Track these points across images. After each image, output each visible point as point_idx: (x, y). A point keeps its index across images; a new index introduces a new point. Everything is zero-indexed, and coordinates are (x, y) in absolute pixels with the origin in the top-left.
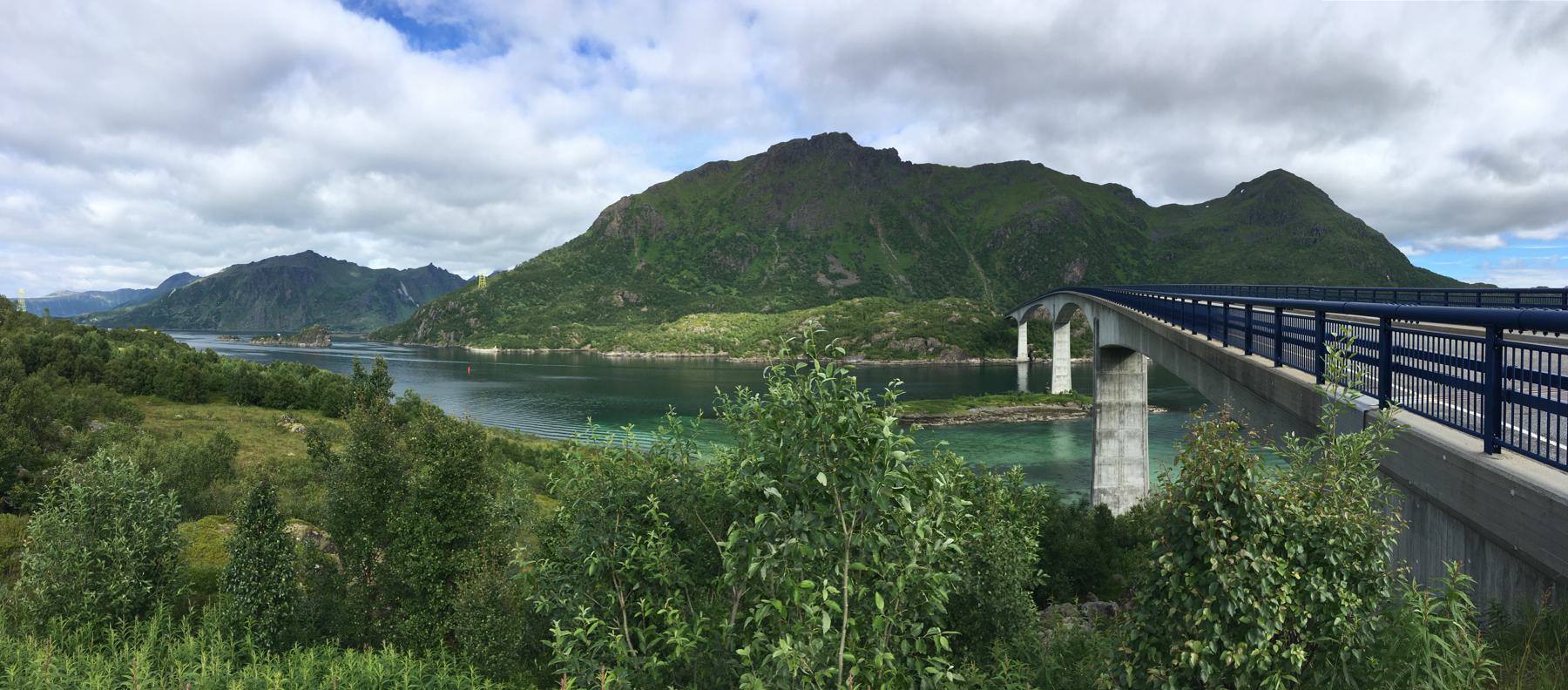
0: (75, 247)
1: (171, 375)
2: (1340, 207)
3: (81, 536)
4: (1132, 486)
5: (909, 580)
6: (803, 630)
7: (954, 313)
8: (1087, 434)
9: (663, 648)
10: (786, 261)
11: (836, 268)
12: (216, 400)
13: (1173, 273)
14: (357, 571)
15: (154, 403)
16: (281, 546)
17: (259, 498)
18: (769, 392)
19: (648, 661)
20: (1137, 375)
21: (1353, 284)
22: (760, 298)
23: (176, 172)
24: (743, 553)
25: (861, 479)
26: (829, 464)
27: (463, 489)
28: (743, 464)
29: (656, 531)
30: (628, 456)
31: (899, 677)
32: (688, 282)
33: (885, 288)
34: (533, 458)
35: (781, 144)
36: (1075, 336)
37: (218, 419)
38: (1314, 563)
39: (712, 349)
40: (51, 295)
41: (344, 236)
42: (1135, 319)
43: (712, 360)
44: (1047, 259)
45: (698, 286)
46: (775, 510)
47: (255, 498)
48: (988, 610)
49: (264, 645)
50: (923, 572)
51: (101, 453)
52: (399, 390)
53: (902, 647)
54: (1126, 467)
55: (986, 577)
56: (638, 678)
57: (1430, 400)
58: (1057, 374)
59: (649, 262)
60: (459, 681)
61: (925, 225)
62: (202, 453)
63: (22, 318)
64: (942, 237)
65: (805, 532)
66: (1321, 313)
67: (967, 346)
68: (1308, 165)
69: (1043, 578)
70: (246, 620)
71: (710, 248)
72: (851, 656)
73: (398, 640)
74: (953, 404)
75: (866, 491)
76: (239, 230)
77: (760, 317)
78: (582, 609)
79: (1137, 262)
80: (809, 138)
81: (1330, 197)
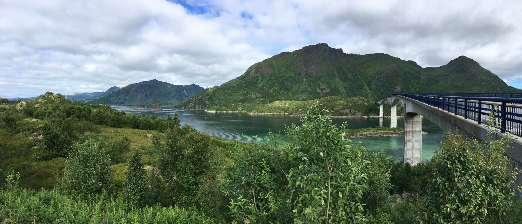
0: (81, 79)
1: (110, 119)
3: (81, 166)
5: (350, 187)
6: (315, 204)
7: (359, 102)
8: (402, 140)
9: (268, 208)
12: (125, 127)
14: (168, 182)
15: (105, 128)
16: (142, 173)
17: (135, 158)
18: (302, 126)
19: (262, 213)
20: (418, 122)
21: (486, 92)
22: (299, 96)
23: (113, 55)
24: (295, 179)
25: (334, 154)
26: (324, 149)
27: (202, 156)
28: (294, 149)
29: (265, 171)
30: (256, 146)
31: (347, 220)
32: (275, 90)
34: (225, 146)
36: (398, 109)
37: (125, 133)
38: (489, 182)
39: (283, 112)
40: (74, 94)
41: (166, 75)
42: (418, 104)
43: (283, 116)
44: (389, 85)
45: (279, 92)
46: (305, 164)
47: (134, 158)
48: (374, 197)
49: (137, 205)
50: (354, 185)
51: (86, 142)
52: (182, 124)
53: (348, 210)
54: (415, 151)
55: (373, 186)
56: (259, 218)
57: (519, 130)
58: (392, 121)
59: (264, 84)
60: (199, 218)
61: (351, 73)
62: (119, 143)
63: (66, 101)
64: (356, 77)
65: (316, 172)
66: (480, 100)
68: (472, 54)
69: (391, 186)
70: (131, 197)
71: (283, 80)
72: (331, 213)
73: (181, 204)
74: (359, 130)
75: (336, 158)
76: (133, 73)
77: (299, 102)
78: (241, 196)
79: (418, 85)
80: (315, 45)
81: (479, 64)
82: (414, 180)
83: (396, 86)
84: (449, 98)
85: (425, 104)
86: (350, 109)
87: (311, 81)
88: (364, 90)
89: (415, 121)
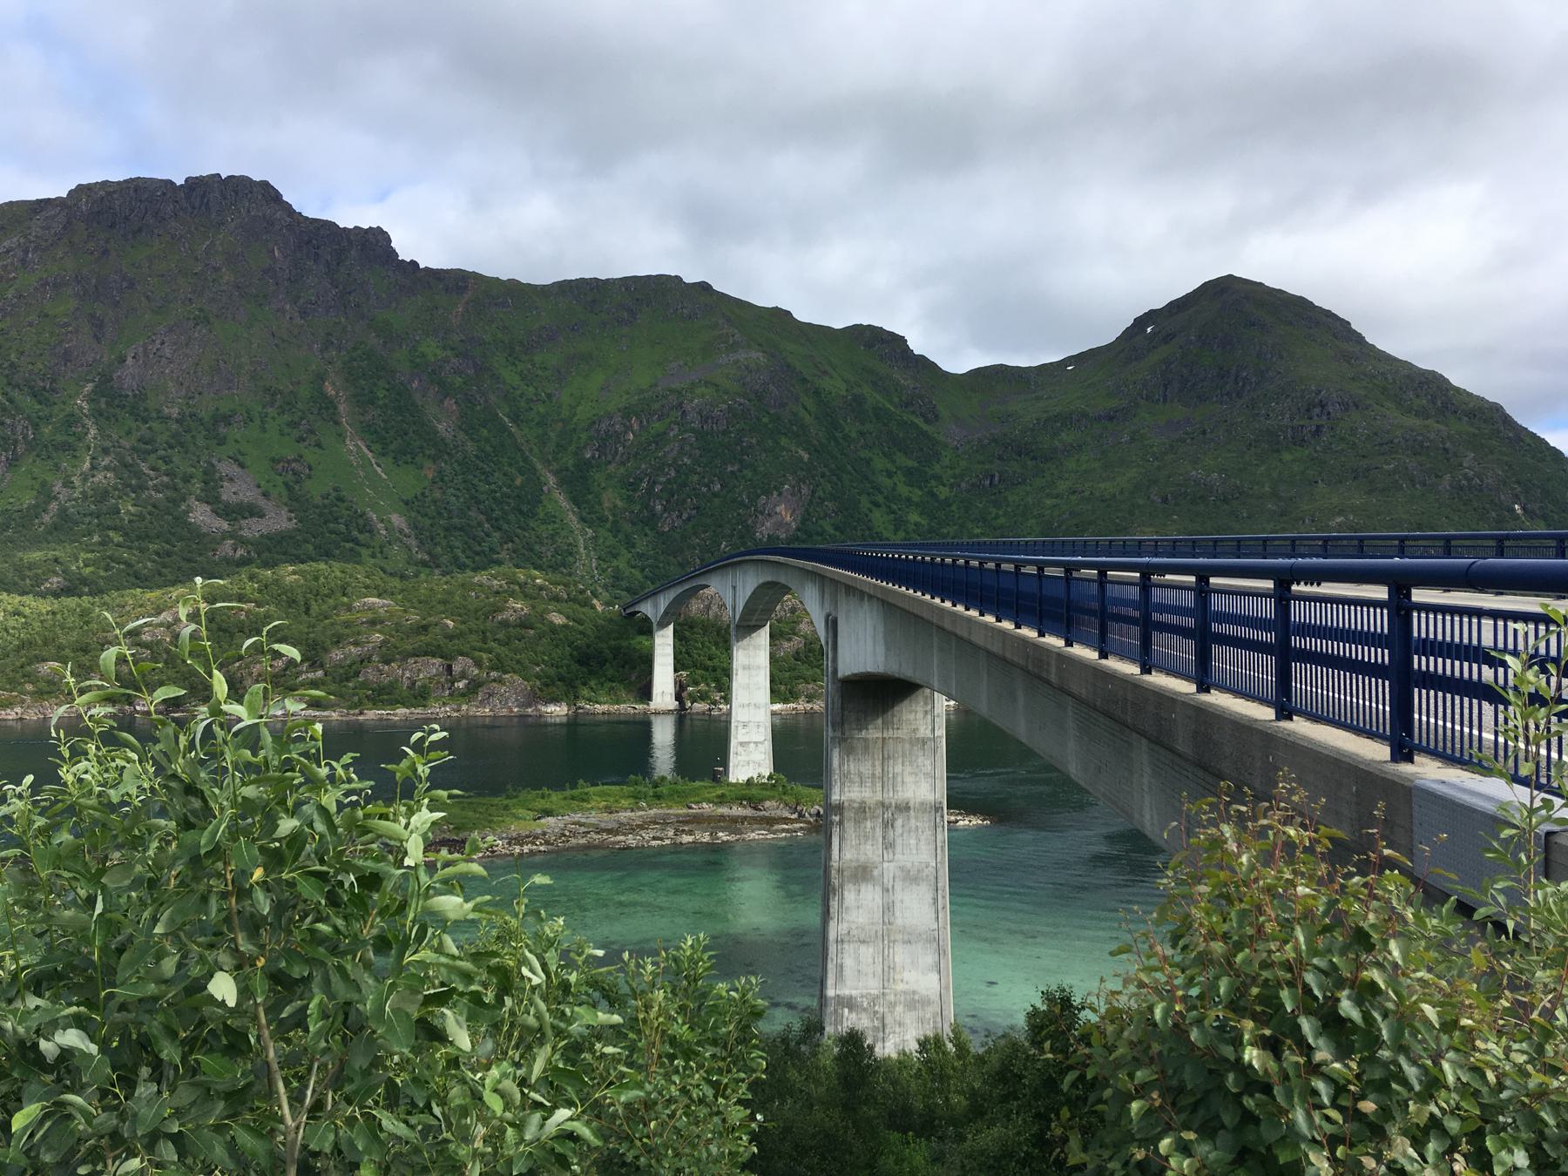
2: (1380, 346)
4: (914, 992)
10: (107, 468)
11: (237, 491)
13: (997, 517)
20: (924, 742)
25: (335, 979)
26: (245, 946)
33: (357, 543)
35: (106, 183)
58: (741, 738)
64: (485, 433)
67: (538, 677)
80: (180, 181)
82: (899, 1161)
83: (768, 493)
84: (1146, 571)
85: (973, 613)
86: (448, 657)
87: (146, 446)
88: (544, 522)
89: (899, 734)
